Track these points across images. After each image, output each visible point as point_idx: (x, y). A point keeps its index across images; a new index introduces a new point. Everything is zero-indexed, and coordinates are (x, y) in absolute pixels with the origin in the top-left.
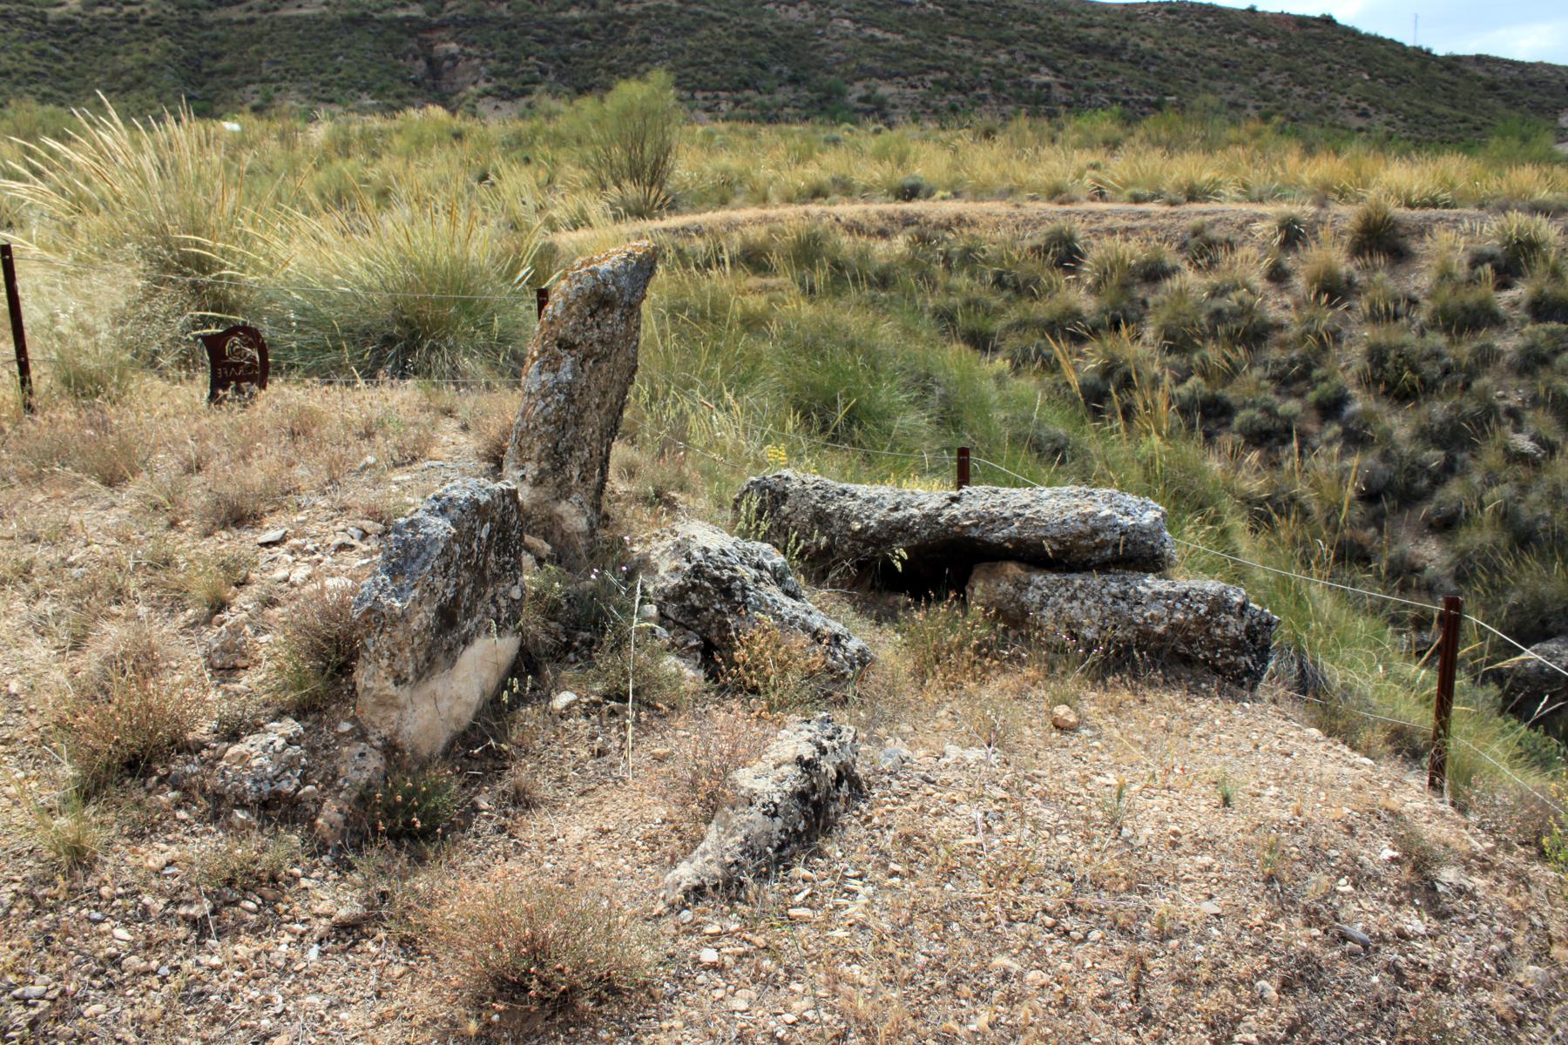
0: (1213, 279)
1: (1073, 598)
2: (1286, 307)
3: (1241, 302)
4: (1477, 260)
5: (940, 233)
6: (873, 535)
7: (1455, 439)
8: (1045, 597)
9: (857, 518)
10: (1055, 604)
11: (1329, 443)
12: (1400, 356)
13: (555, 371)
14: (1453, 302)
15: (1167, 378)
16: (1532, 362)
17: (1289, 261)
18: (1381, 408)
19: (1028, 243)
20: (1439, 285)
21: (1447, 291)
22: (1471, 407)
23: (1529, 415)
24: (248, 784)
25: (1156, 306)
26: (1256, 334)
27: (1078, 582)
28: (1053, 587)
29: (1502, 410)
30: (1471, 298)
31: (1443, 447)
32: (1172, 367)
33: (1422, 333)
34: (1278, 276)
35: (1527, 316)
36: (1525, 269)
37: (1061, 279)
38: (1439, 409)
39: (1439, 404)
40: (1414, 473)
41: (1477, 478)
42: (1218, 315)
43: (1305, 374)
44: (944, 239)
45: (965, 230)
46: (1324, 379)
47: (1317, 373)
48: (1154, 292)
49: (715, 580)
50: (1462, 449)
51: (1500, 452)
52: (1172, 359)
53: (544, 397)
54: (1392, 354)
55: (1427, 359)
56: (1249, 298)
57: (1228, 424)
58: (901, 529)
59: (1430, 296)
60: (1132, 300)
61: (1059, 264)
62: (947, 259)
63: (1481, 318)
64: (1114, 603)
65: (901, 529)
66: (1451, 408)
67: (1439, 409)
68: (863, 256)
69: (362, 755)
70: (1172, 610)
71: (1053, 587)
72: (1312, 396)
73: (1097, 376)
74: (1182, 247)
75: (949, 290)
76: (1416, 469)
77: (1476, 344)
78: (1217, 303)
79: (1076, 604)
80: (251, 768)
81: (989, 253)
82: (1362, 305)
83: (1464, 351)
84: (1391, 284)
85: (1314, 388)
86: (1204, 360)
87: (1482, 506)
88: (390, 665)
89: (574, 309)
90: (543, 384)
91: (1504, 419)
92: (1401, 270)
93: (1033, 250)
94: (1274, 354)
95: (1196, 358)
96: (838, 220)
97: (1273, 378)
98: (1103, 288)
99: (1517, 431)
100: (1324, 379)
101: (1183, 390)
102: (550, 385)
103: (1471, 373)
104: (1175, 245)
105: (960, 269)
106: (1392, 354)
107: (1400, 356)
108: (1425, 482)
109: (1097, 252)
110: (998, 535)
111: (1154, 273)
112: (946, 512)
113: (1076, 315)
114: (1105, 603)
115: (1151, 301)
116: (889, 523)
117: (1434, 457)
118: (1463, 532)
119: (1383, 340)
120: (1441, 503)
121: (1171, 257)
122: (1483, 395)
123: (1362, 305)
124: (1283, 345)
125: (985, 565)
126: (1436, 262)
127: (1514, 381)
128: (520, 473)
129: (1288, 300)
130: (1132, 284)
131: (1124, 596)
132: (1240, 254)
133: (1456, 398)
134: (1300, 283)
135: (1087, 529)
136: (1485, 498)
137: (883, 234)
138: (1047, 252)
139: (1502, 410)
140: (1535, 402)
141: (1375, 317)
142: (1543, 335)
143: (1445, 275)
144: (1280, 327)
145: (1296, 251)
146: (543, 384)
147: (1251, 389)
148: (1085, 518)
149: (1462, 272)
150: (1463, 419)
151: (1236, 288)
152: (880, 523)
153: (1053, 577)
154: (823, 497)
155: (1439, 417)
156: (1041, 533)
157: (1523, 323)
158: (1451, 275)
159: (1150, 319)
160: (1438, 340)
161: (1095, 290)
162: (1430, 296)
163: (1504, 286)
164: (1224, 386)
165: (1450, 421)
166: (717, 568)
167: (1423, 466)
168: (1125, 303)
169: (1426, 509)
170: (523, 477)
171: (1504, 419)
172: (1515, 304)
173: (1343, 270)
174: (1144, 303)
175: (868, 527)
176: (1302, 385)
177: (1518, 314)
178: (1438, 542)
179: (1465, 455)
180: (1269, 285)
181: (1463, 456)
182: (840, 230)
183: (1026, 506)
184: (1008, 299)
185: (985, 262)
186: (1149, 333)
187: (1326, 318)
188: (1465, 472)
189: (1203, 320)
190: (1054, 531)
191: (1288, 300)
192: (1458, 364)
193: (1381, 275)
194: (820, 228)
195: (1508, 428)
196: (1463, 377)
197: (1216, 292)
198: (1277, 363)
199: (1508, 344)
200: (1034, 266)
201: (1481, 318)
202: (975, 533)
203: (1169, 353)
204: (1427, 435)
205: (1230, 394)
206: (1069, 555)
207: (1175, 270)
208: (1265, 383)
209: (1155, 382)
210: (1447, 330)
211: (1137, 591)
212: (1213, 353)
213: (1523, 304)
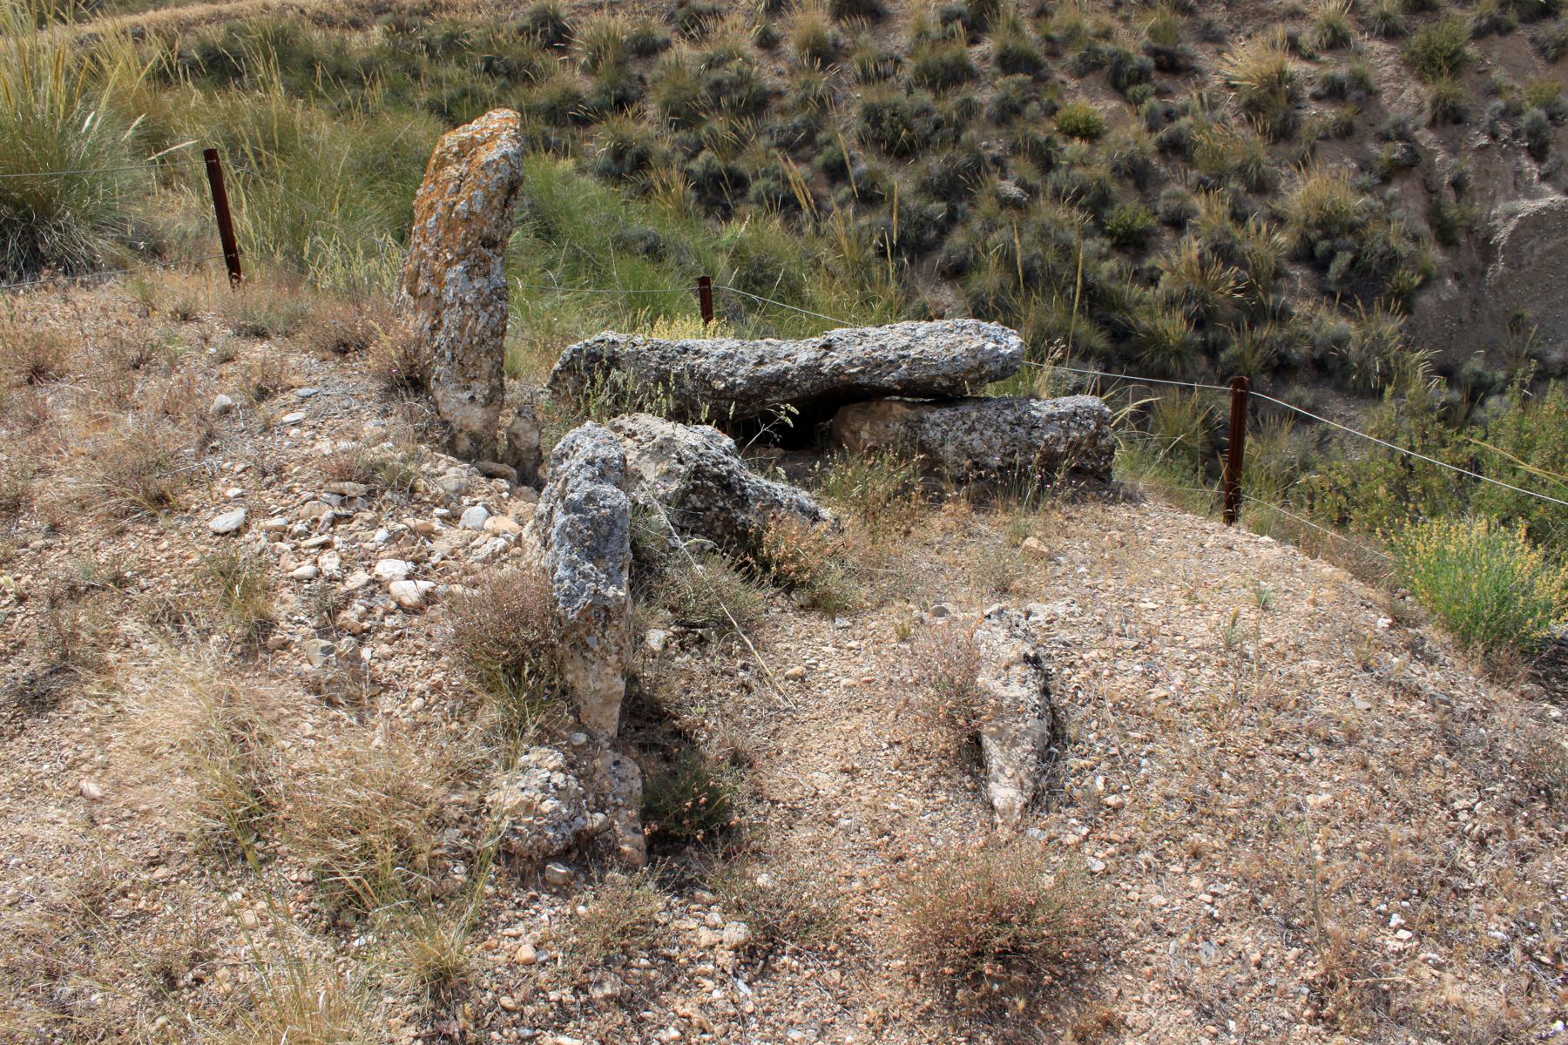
0: (708, 50)
1: (970, 431)
2: (780, 74)
3: (739, 73)
4: (948, 18)
5: (417, 20)
6: (742, 393)
7: (953, 189)
8: (945, 433)
9: (717, 376)
10: (955, 438)
11: (842, 205)
12: (894, 115)
13: (486, 275)
14: (933, 60)
15: (679, 156)
16: (1007, 113)
17: (776, 27)
18: (884, 166)
19: (514, 25)
20: (917, 43)
21: (926, 49)
22: (963, 159)
23: (1012, 162)
24: (551, 834)
25: (655, 81)
26: (758, 103)
27: (974, 415)
28: (950, 422)
29: (988, 160)
30: (948, 54)
31: (944, 199)
32: (682, 143)
33: (910, 92)
34: (768, 42)
35: (997, 69)
36: (991, 26)
37: (556, 61)
38: (934, 163)
39: (935, 159)
40: (923, 226)
41: (977, 225)
42: (717, 86)
43: (809, 139)
44: (423, 26)
45: (444, 15)
46: (828, 143)
47: (821, 137)
48: (649, 68)
49: (717, 478)
50: (961, 200)
51: (993, 199)
52: (682, 134)
53: (484, 306)
54: (887, 113)
55: (917, 115)
56: (746, 68)
57: (743, 195)
58: (777, 383)
59: (911, 54)
60: (629, 78)
61: (549, 45)
62: (430, 49)
63: (955, 75)
64: (1012, 430)
65: (777, 383)
66: (946, 162)
67: (934, 163)
68: (340, 50)
69: (616, 763)
70: (1067, 430)
71: (950, 422)
72: (819, 160)
73: (609, 159)
74: (671, 18)
75: (438, 82)
76: (924, 222)
77: (958, 99)
78: (716, 75)
79: (975, 435)
80: (544, 815)
81: (475, 38)
82: (853, 66)
83: (948, 105)
84: (874, 45)
85: (820, 152)
86: (712, 133)
87: (986, 251)
88: (619, 660)
89: (495, 202)
90: (479, 292)
91: (991, 168)
92: (881, 30)
93: (521, 31)
94: (778, 121)
95: (703, 131)
96: (302, 11)
97: (780, 146)
98: (601, 66)
99: (1004, 178)
100: (828, 143)
101: (696, 166)
102: (487, 292)
103: (959, 129)
104: (664, 17)
105: (448, 58)
106: (887, 113)
107: (894, 115)
108: (933, 234)
109: (586, 29)
110: (889, 379)
111: (647, 48)
112: (827, 361)
113: (576, 98)
114: (1004, 432)
115: (648, 76)
116: (760, 378)
117: (938, 209)
118: (974, 277)
119: (876, 99)
120: (949, 253)
121: (661, 31)
122: (971, 148)
123: (853, 66)
124: (783, 111)
125: (856, 407)
126: (911, 21)
127: (994, 132)
128: (466, 395)
129: (782, 66)
130: (626, 61)
131: (1019, 422)
132: (729, 22)
133: (949, 151)
134: (790, 48)
135: (975, 363)
136: (988, 243)
137: (356, 25)
138: (535, 33)
139: (988, 160)
140: (1015, 150)
141: (865, 79)
142: (1012, 86)
143: (921, 34)
144: (779, 94)
145: (781, 16)
146: (479, 292)
147: (760, 156)
148: (973, 353)
149: (935, 29)
150: (957, 171)
151: (731, 58)
152: (749, 379)
153: (948, 412)
154: (663, 358)
155: (937, 171)
156: (933, 372)
157: (995, 76)
158: (927, 34)
159: (651, 96)
160: (924, 97)
161: (591, 69)
162: (910, 55)
163: (974, 41)
164: (734, 158)
165: (947, 174)
166: (714, 465)
167: (929, 218)
168: (623, 81)
169: (939, 258)
170: (472, 398)
171: (991, 168)
172: (985, 59)
173: (829, 32)
174: (641, 79)
175: (734, 385)
176: (808, 150)
177: (989, 68)
178: (953, 287)
179: (965, 204)
180: (761, 52)
181: (963, 206)
182: (308, 23)
183: (907, 347)
184: (503, 87)
185: (471, 48)
186: (653, 109)
187: (822, 82)
188: (965, 222)
189: (704, 92)
190: (946, 369)
191: (782, 66)
192: (949, 118)
193: (864, 36)
194: (285, 23)
195: (996, 177)
196: (949, 130)
197: (713, 63)
198: (782, 131)
199: (985, 97)
200: (521, 50)
201: (955, 75)
202: (864, 380)
203: (676, 130)
204: (928, 189)
205: (742, 165)
206: (942, 391)
207: (667, 44)
208: (774, 151)
209: (667, 161)
210: (932, 86)
211: (1031, 416)
212: (718, 124)
213: (992, 58)
